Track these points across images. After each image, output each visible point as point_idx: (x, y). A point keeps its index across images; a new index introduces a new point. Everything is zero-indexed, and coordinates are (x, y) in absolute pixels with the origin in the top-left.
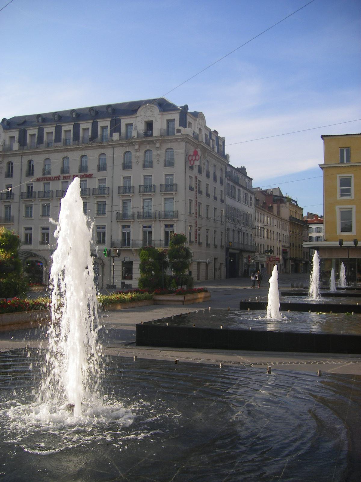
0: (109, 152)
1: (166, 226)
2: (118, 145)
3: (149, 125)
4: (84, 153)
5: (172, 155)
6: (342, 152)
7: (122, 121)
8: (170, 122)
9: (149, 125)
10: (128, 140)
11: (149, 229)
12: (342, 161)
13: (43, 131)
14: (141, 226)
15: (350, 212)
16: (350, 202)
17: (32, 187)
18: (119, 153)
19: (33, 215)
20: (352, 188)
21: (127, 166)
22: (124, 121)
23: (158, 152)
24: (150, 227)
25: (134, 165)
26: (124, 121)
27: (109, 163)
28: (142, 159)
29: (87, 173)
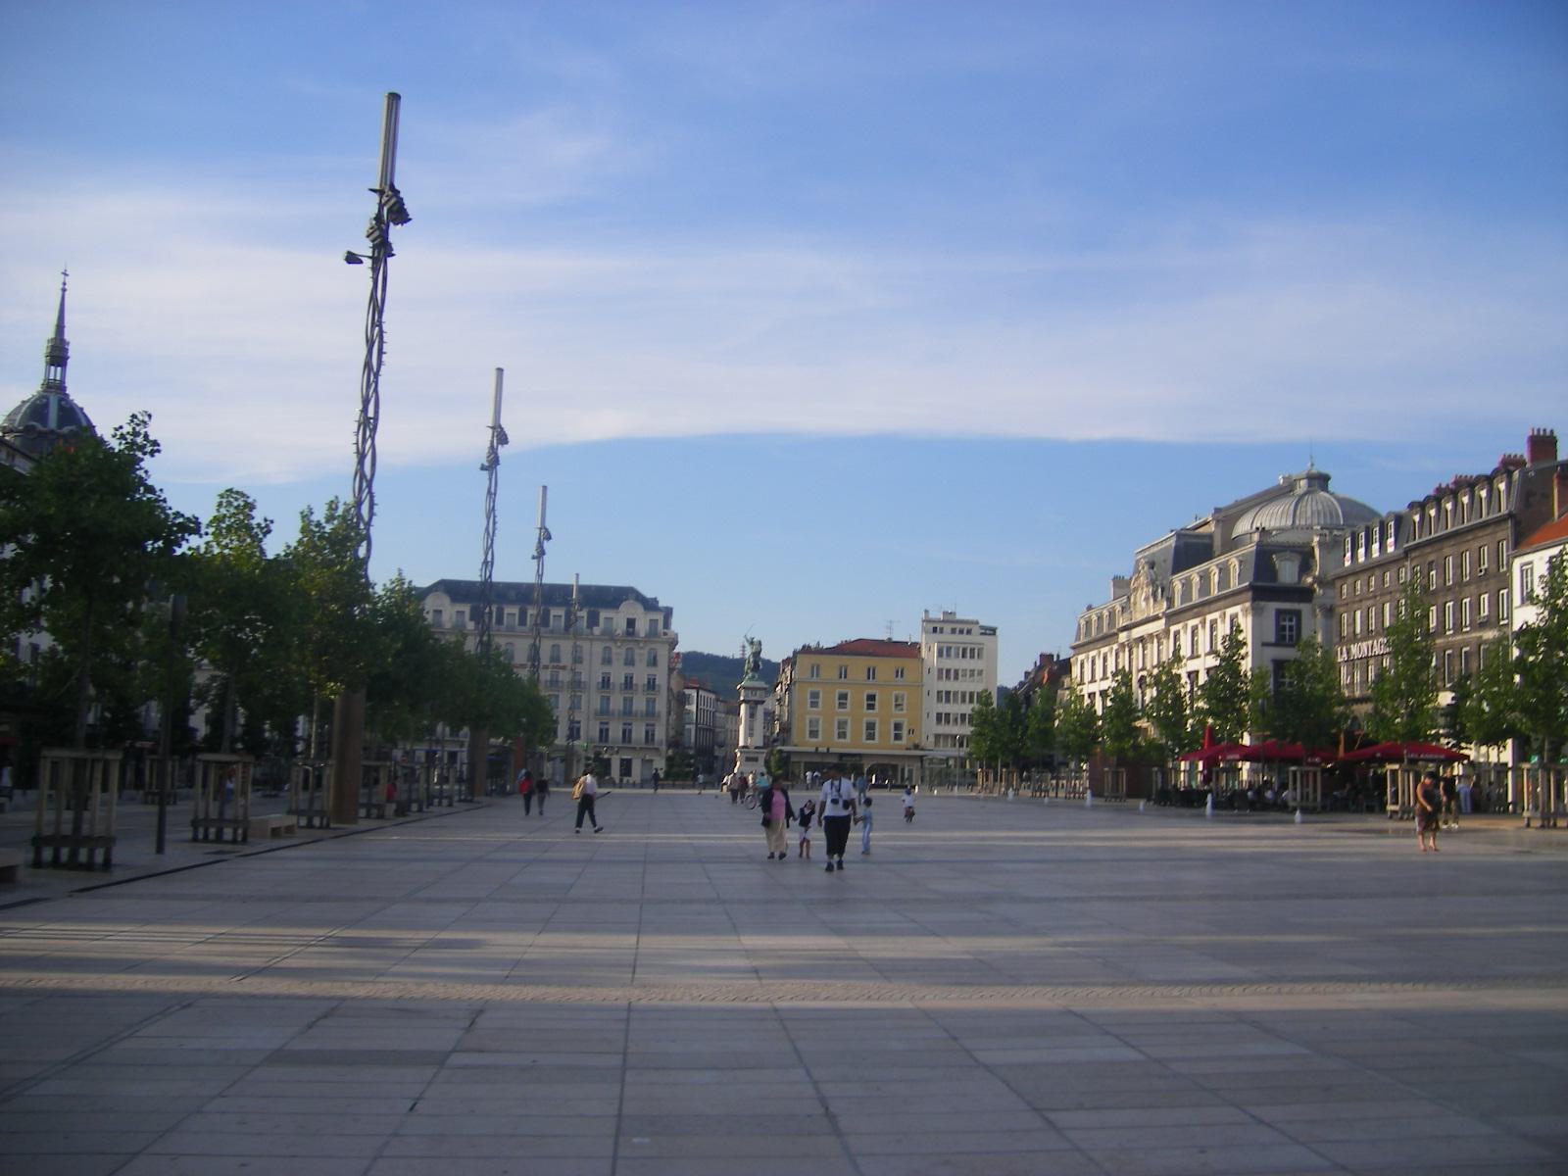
0: (585, 645)
1: (647, 725)
2: (599, 639)
3: (631, 623)
4: (556, 642)
5: (559, 651)
6: (813, 668)
7: (601, 614)
8: (653, 622)
9: (631, 623)
10: (609, 635)
11: (606, 726)
12: (869, 678)
13: (526, 613)
14: (644, 724)
15: (817, 721)
16: (819, 713)
17: (632, 678)
18: (598, 648)
19: (645, 703)
20: (877, 703)
21: (607, 661)
22: (604, 614)
23: (642, 651)
24: (630, 724)
25: (637, 663)
26: (604, 614)
27: (586, 657)
28: (623, 657)
29: (561, 664)
